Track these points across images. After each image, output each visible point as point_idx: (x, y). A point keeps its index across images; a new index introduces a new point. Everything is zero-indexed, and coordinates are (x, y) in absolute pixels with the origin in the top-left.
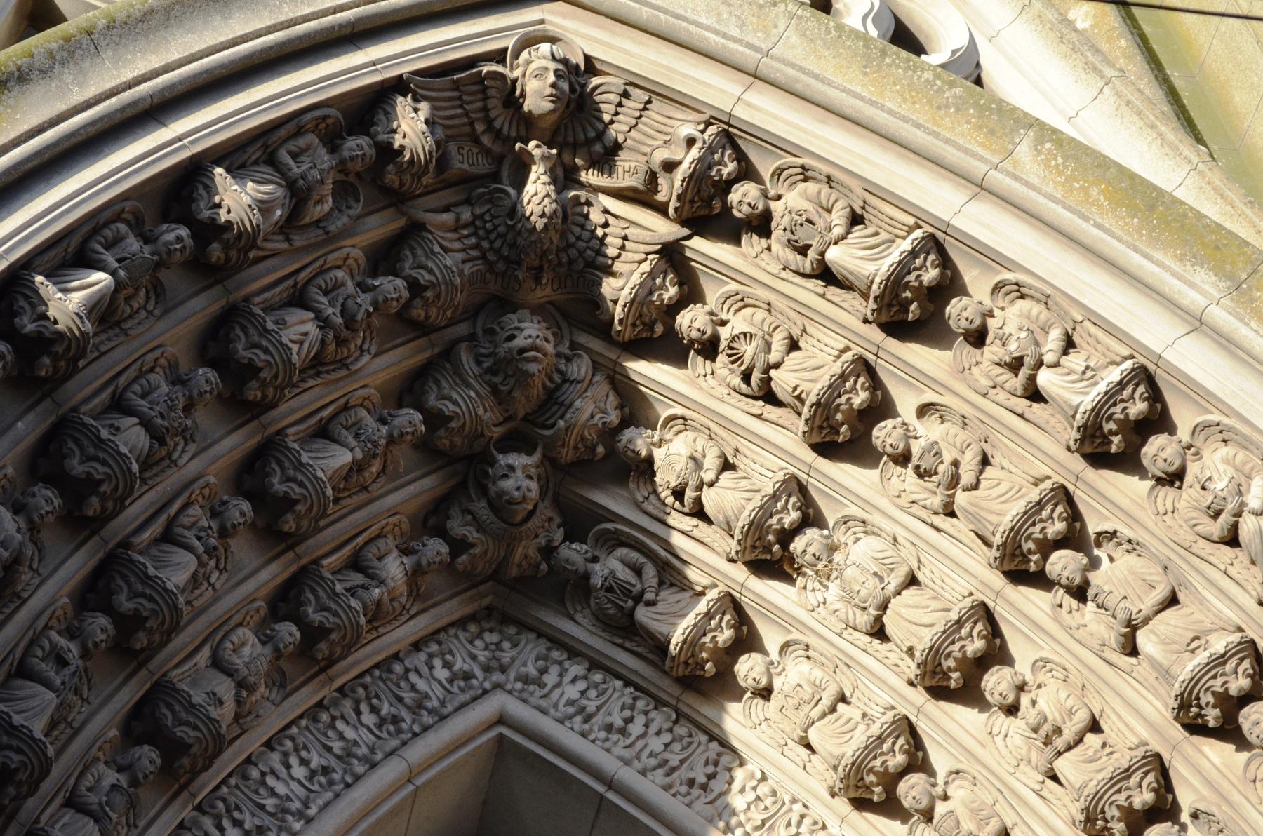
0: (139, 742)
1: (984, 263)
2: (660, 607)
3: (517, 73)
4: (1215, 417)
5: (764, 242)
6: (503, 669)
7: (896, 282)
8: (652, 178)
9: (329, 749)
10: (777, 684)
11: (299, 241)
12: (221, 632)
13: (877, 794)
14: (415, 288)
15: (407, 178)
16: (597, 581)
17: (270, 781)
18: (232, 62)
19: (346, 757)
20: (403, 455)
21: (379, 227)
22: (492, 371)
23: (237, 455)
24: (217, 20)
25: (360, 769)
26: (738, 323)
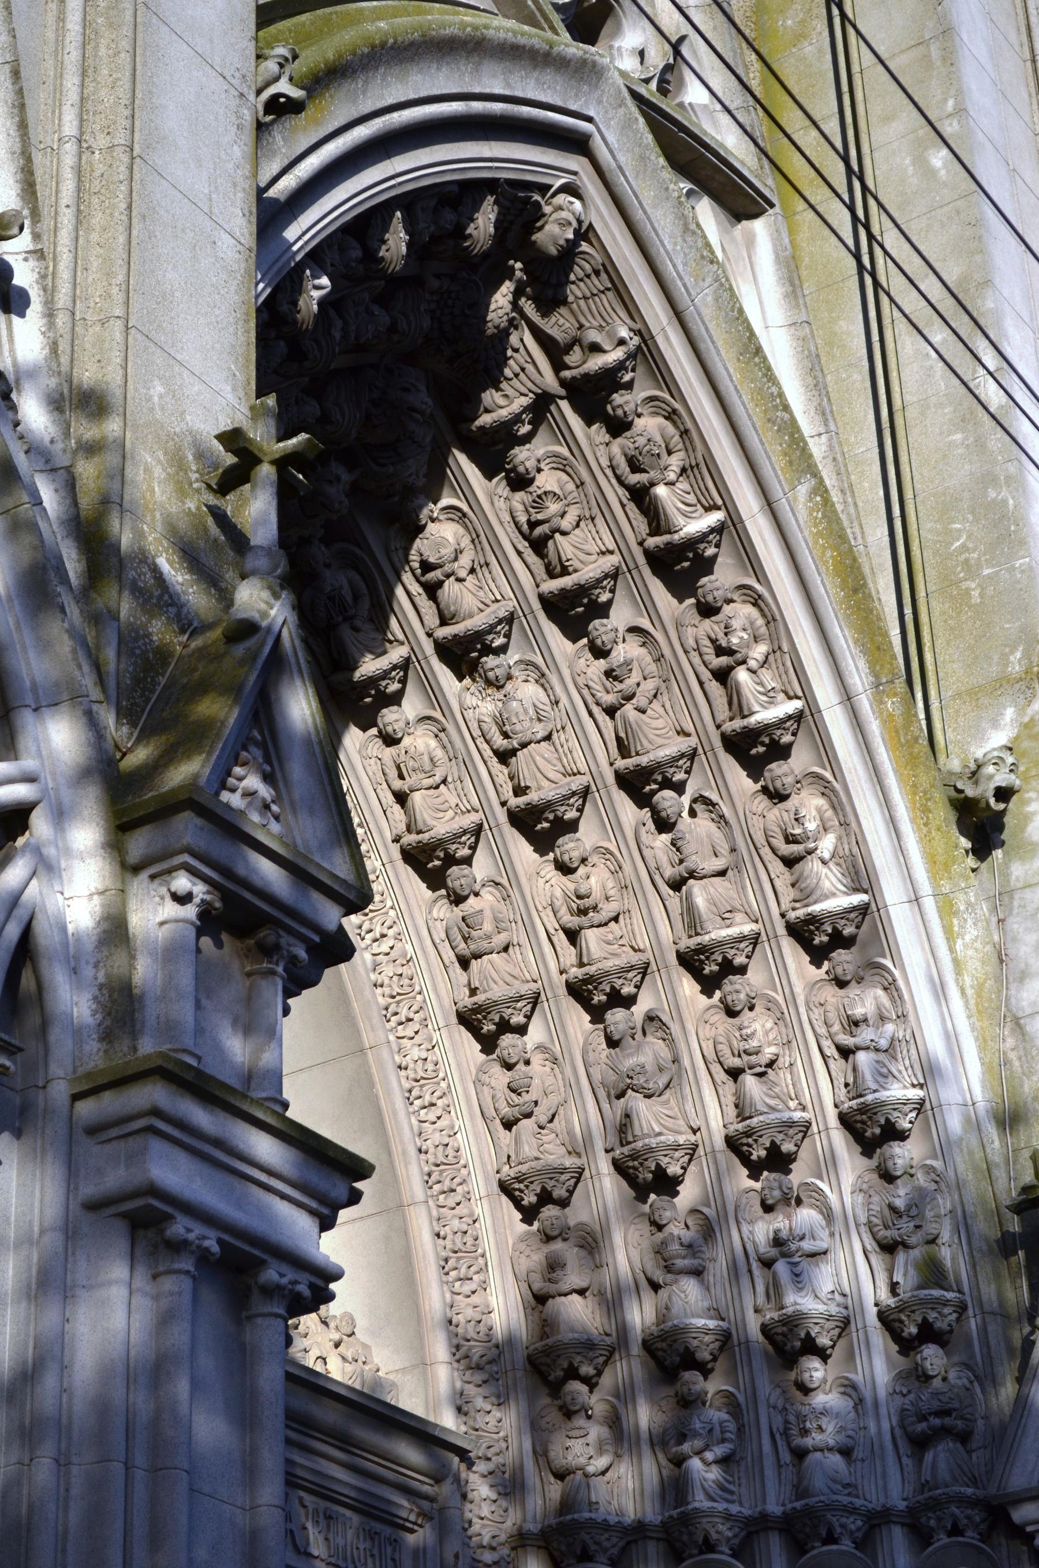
1: (743, 561)
4: (828, 775)
5: (607, 438)
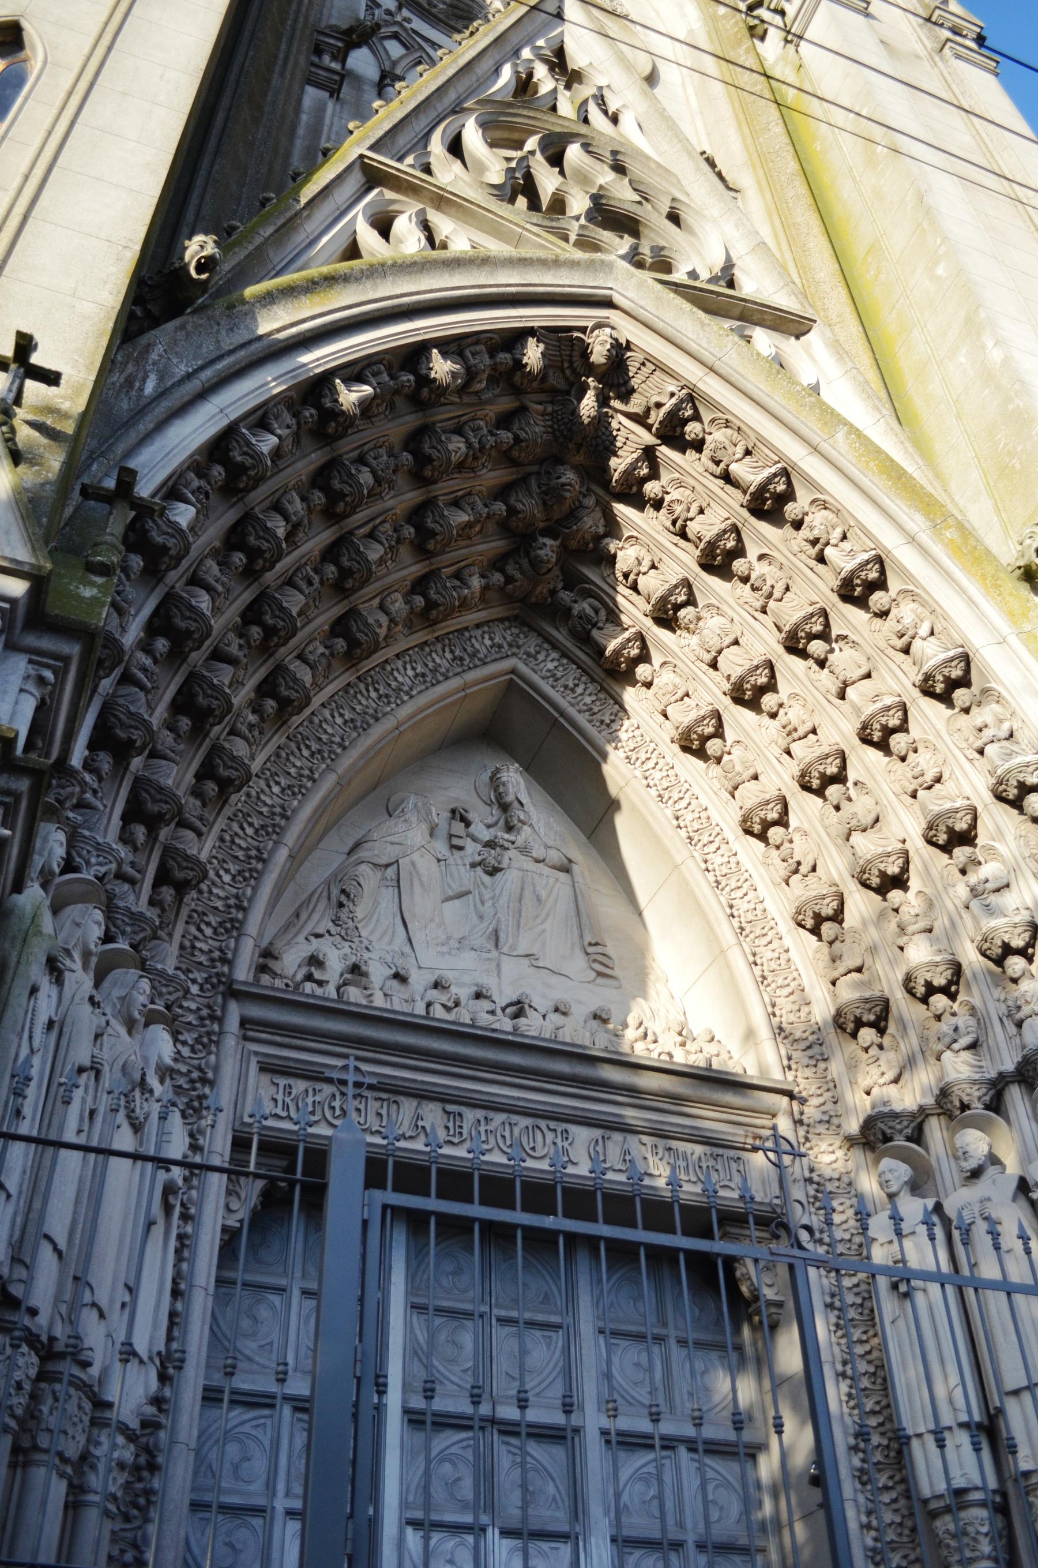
0: (337, 636)
2: (605, 631)
3: (590, 341)
4: (912, 588)
6: (518, 647)
7: (763, 488)
8: (648, 410)
9: (427, 665)
10: (656, 681)
11: (466, 399)
12: (386, 592)
13: (696, 745)
14: (517, 439)
15: (525, 381)
16: (575, 612)
17: (396, 673)
18: (452, 298)
19: (434, 671)
20: (491, 526)
21: (505, 404)
22: (546, 493)
23: (412, 503)
24: (446, 276)
25: (441, 678)
26: (675, 494)
